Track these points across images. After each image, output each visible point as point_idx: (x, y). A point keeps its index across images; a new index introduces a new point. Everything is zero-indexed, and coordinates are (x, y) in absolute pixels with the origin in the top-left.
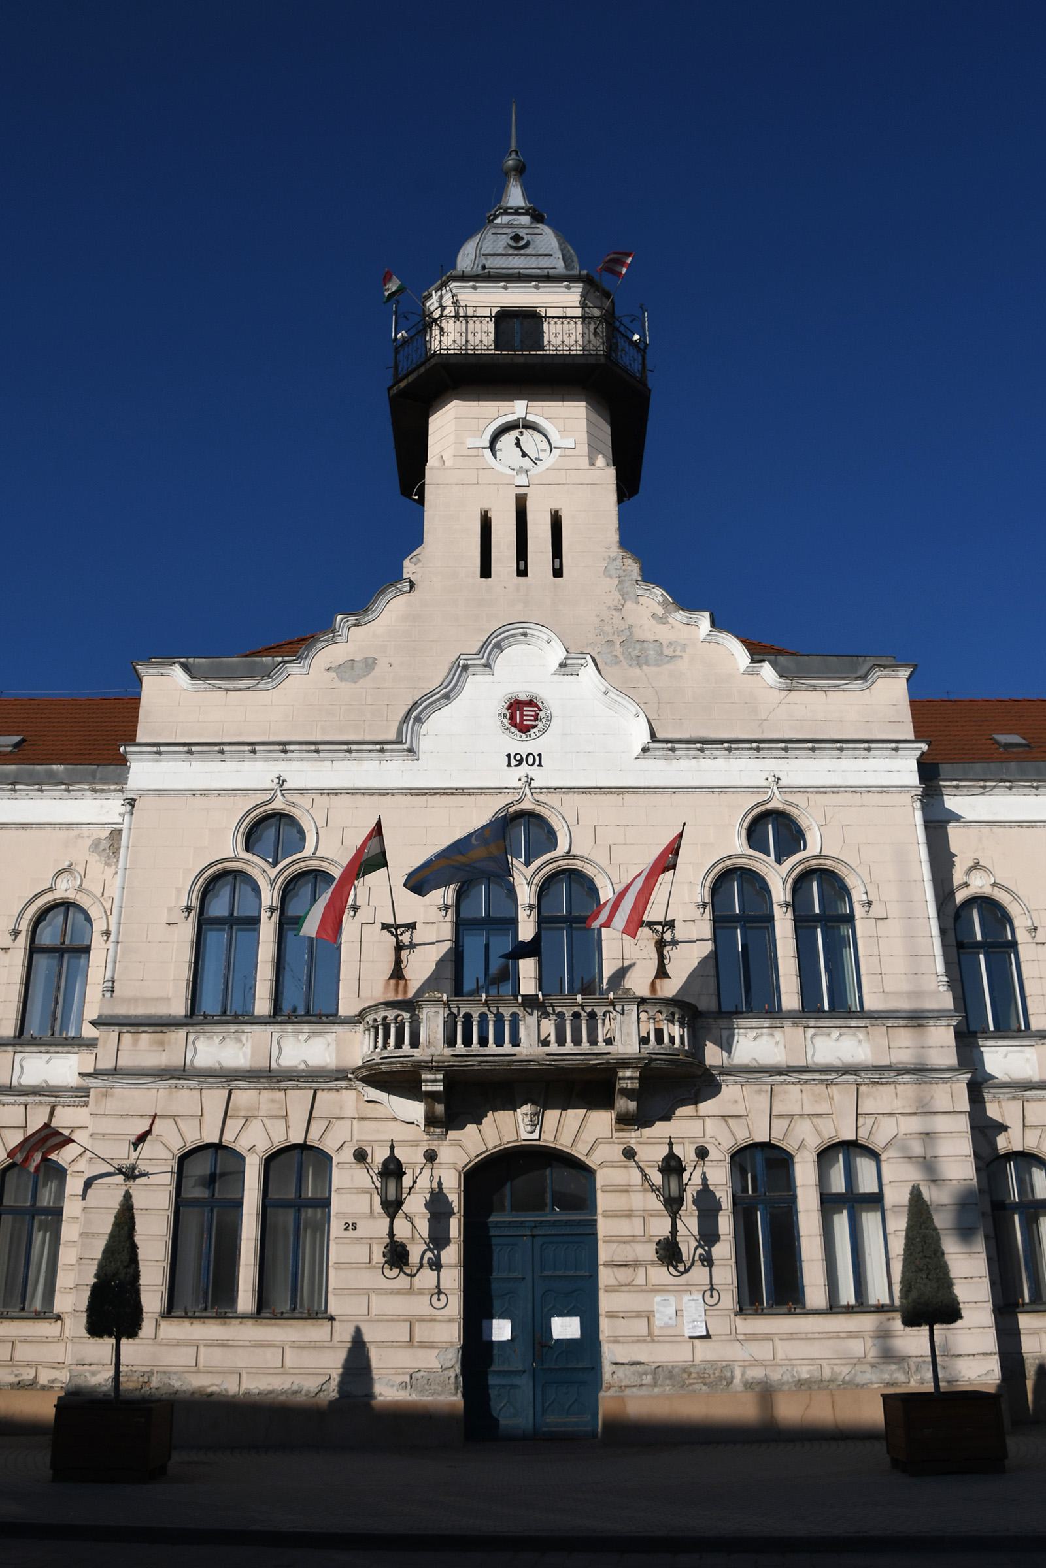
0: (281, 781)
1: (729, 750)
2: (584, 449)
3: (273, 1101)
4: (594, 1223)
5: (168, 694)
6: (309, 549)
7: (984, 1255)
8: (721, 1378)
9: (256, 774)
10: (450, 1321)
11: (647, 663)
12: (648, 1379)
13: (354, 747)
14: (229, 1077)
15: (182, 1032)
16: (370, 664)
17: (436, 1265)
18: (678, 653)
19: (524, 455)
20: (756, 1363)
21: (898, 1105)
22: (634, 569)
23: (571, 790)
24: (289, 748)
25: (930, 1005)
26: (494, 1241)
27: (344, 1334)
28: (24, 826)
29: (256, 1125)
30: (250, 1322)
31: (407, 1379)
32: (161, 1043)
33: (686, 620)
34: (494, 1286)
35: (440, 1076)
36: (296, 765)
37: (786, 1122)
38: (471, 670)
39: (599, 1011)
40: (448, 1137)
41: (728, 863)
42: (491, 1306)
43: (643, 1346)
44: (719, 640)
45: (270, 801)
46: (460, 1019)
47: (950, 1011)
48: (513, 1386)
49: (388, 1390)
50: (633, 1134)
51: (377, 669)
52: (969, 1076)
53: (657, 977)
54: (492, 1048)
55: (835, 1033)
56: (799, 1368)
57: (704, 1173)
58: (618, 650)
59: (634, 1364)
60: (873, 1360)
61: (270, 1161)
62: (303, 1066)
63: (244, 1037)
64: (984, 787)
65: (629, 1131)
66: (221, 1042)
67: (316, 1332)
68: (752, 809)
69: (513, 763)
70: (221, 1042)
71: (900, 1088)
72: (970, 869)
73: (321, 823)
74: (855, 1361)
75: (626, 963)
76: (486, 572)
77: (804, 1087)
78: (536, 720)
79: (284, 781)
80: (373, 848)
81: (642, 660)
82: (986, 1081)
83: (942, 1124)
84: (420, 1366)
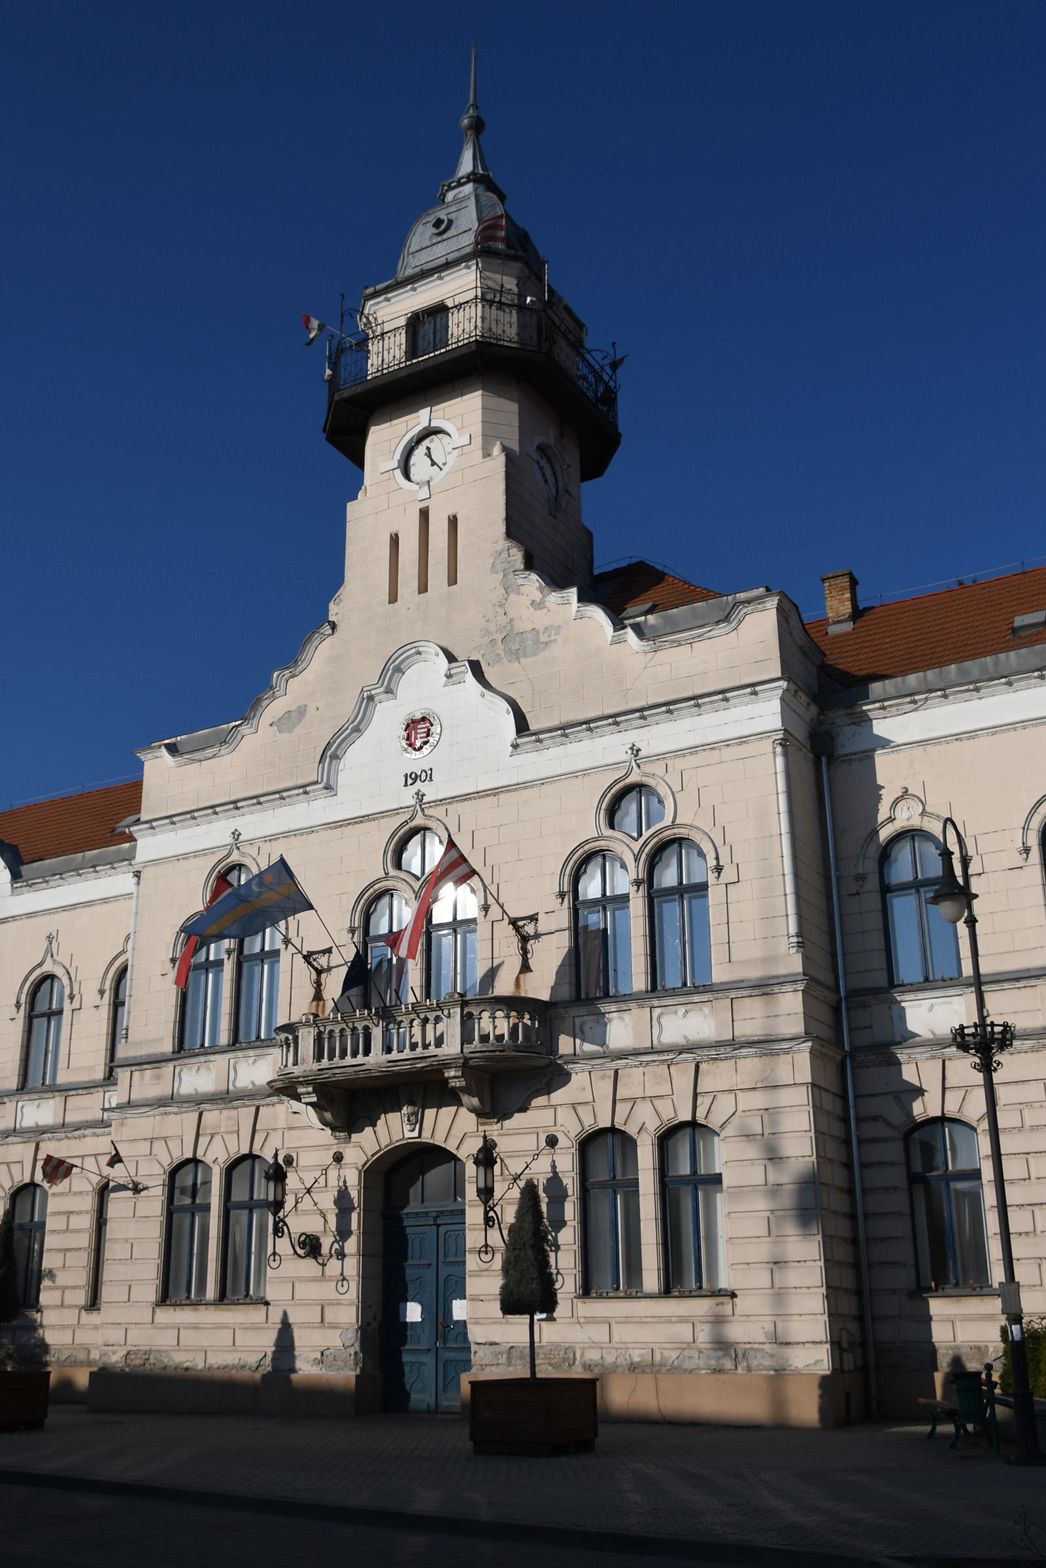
0: (635, 751)
1: (670, 712)
2: (478, 441)
3: (229, 1118)
4: (463, 1212)
5: (164, 776)
6: (247, 617)
7: (819, 1238)
8: (564, 1360)
9: (607, 750)
10: (351, 1304)
11: (525, 656)
12: (503, 1359)
13: (285, 794)
14: (200, 1101)
15: (171, 1065)
16: (302, 711)
17: (341, 1255)
18: (553, 638)
19: (433, 463)
20: (594, 1345)
21: (743, 1080)
22: (517, 556)
23: (453, 799)
24: (239, 804)
25: (781, 970)
26: (408, 1230)
27: (276, 1318)
28: (105, 900)
29: (218, 1139)
30: (212, 1307)
31: (318, 1355)
32: (158, 1077)
33: (560, 601)
34: (408, 1272)
35: (310, 1089)
36: (249, 818)
37: (629, 1105)
38: (376, 699)
39: (431, 1016)
40: (353, 1140)
41: (586, 848)
42: (406, 1291)
43: (499, 1326)
44: (589, 614)
45: (627, 775)
46: (326, 1036)
47: (799, 974)
48: (422, 1364)
49: (306, 1368)
50: (495, 1127)
51: (307, 716)
52: (810, 1044)
53: (520, 973)
54: (349, 1060)
55: (681, 1010)
56: (631, 1352)
57: (554, 1161)
58: (500, 646)
59: (491, 1344)
60: (703, 1346)
61: (230, 1170)
62: (251, 1086)
63: (211, 1065)
64: (914, 702)
65: (490, 1124)
66: (197, 1071)
67: (256, 1315)
68: (610, 787)
69: (410, 781)
70: (197, 1071)
71: (741, 1062)
72: (896, 802)
73: (676, 787)
74: (685, 1346)
75: (496, 963)
76: (393, 598)
77: (647, 1069)
78: (428, 735)
79: (638, 750)
80: (453, 855)
81: (521, 653)
82: (906, 1040)
83: (786, 1097)
84: (329, 1344)
